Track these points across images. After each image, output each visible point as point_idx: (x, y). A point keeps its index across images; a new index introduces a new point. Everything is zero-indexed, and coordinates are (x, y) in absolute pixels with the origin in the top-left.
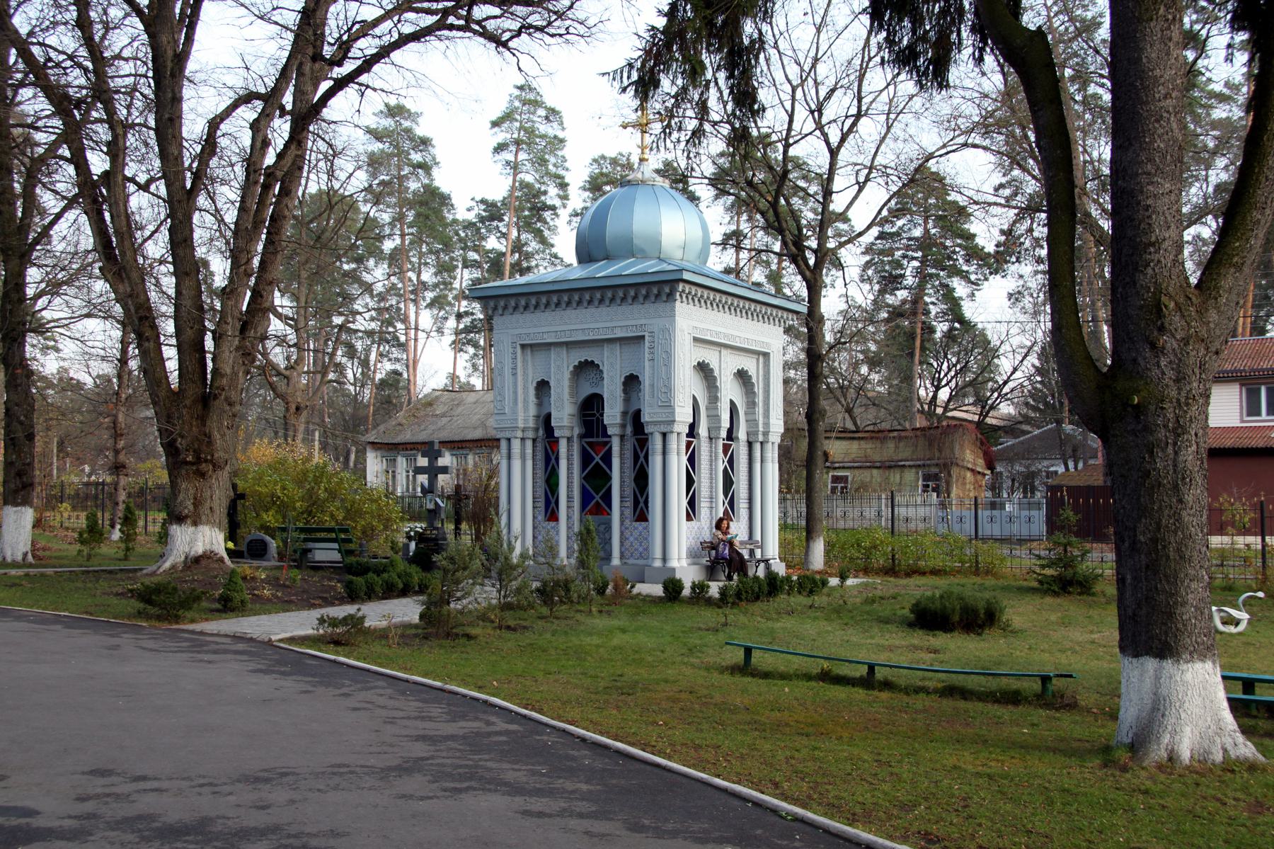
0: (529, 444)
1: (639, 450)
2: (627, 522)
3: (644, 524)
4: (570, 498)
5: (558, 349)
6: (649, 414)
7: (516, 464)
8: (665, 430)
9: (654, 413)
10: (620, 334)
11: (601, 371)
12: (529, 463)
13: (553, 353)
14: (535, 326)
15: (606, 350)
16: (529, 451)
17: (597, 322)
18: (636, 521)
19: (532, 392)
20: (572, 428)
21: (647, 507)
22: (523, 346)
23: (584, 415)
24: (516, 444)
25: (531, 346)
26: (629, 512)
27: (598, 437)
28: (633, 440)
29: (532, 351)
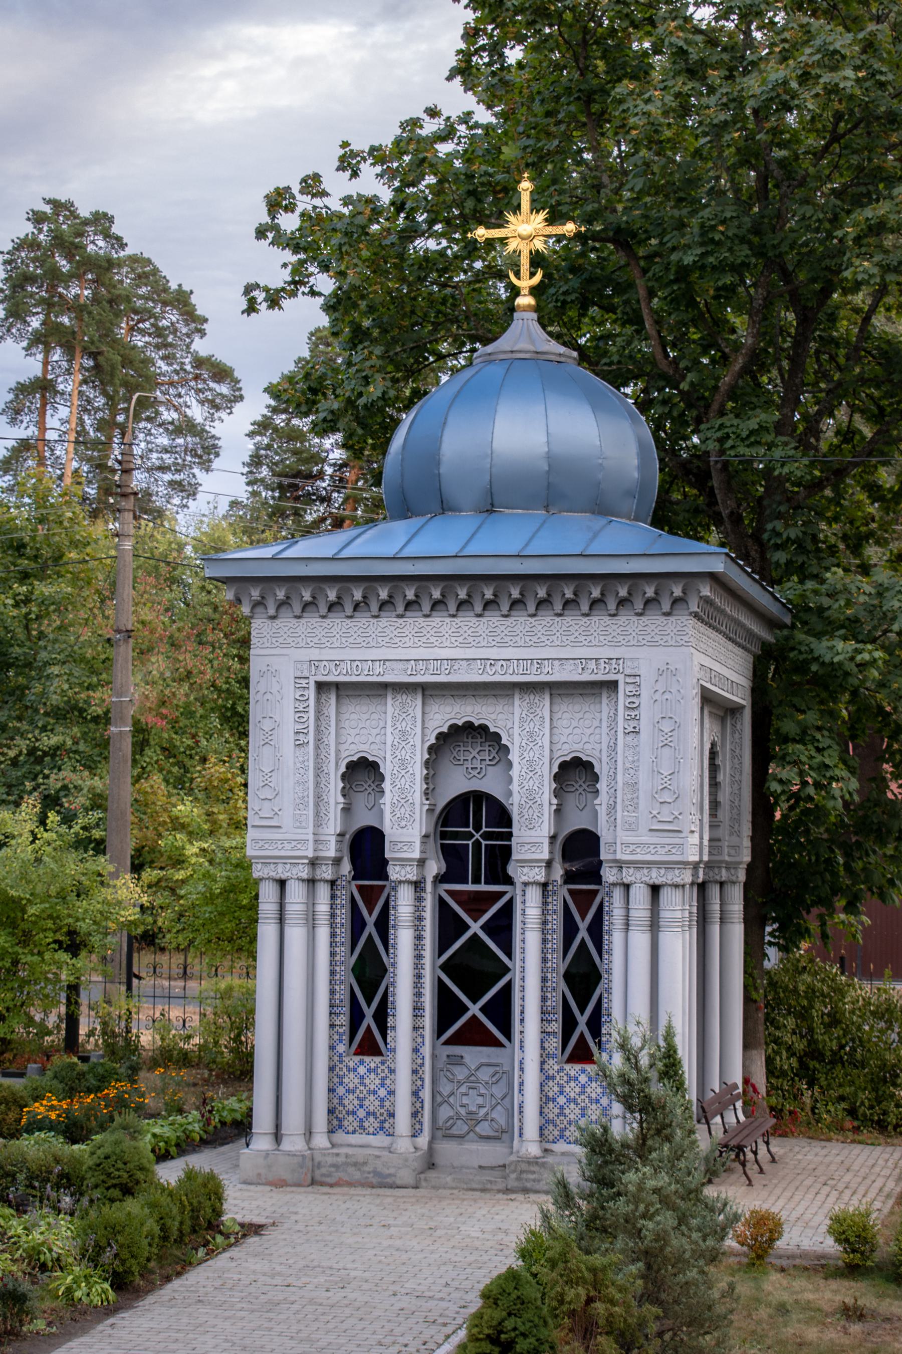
0: (323, 892)
1: (365, 912)
2: (553, 1066)
3: (372, 1061)
4: (417, 1010)
5: (403, 698)
6: (255, 841)
7: (296, 935)
8: (658, 882)
9: (638, 845)
10: (558, 676)
11: (506, 750)
12: (323, 934)
13: (392, 705)
14: (356, 646)
15: (519, 706)
16: (323, 907)
17: (502, 645)
18: (571, 1060)
19: (335, 785)
20: (421, 862)
21: (384, 1029)
22: (321, 687)
23: (444, 835)
24: (296, 893)
25: (338, 686)
26: (555, 1043)
27: (477, 881)
28: (564, 892)
29: (338, 697)
